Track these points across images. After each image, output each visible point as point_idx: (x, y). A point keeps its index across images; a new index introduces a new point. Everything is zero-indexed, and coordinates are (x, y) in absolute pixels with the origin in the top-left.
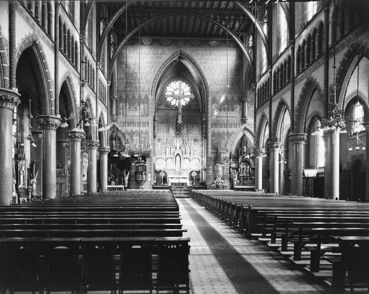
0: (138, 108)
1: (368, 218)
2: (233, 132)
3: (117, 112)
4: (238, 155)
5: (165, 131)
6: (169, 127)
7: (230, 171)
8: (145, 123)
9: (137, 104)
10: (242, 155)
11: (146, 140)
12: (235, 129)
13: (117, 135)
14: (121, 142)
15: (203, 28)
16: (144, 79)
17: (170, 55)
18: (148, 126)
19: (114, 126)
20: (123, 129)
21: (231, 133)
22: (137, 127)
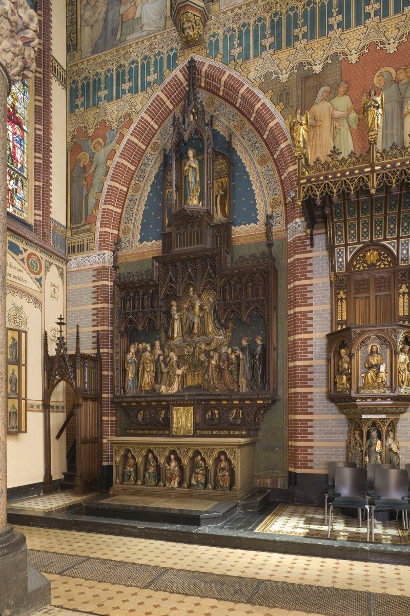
2: (127, 120)
22: (335, 33)
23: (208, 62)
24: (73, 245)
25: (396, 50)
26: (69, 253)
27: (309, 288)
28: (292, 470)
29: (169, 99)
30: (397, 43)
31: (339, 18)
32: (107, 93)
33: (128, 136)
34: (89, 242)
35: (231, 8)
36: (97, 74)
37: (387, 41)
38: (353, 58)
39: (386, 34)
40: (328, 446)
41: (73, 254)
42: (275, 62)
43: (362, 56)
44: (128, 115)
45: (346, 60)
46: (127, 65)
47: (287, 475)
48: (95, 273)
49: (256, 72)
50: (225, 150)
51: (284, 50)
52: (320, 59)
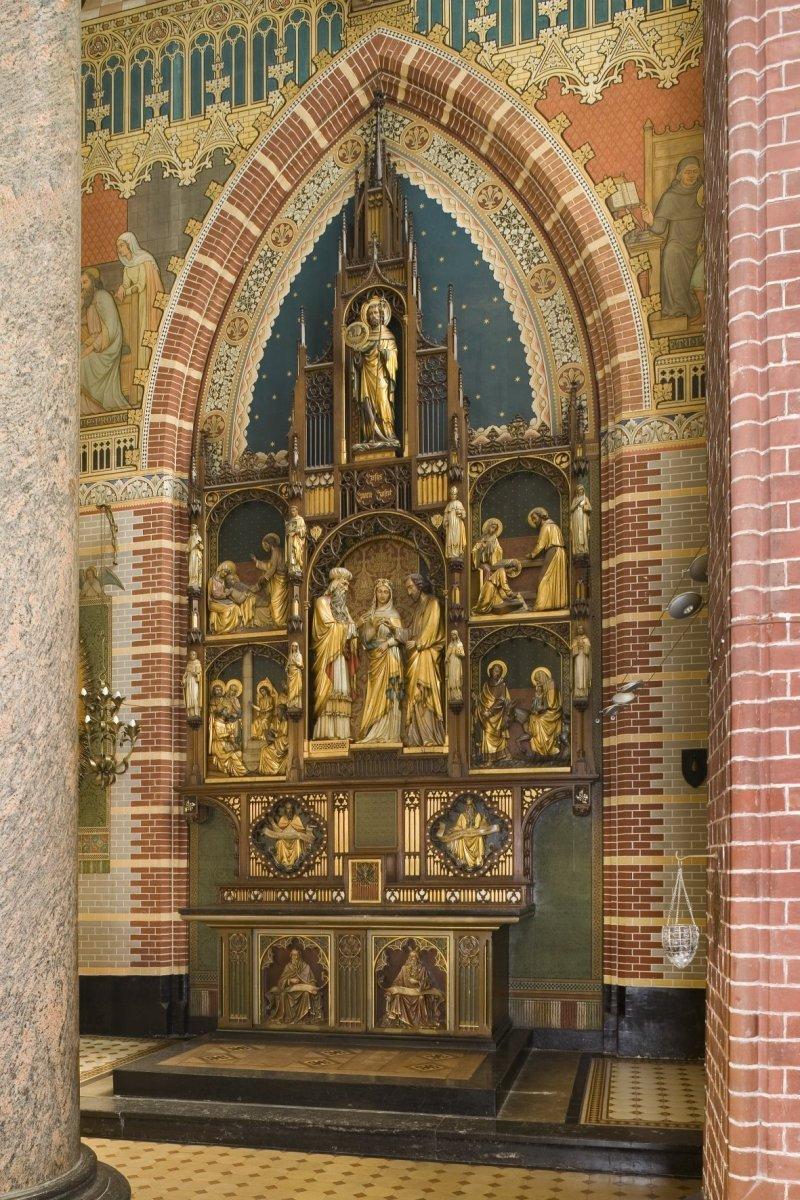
2: (218, 166)
10: (330, 456)
21: (187, 176)
22: (218, 110)
24: (105, 448)
25: (600, 97)
26: (95, 468)
27: (139, 637)
28: (614, 980)
29: (318, 123)
30: (678, 67)
31: (225, 82)
32: (494, 24)
33: (221, 203)
34: (122, 445)
35: (88, 23)
36: (264, 23)
37: (582, 79)
39: (580, 63)
40: (651, 924)
41: (105, 470)
42: (232, 128)
43: (608, 88)
44: (219, 155)
45: (116, 190)
46: (281, 22)
47: (598, 991)
48: (140, 520)
49: (678, 43)
51: (249, 107)
52: (596, 72)
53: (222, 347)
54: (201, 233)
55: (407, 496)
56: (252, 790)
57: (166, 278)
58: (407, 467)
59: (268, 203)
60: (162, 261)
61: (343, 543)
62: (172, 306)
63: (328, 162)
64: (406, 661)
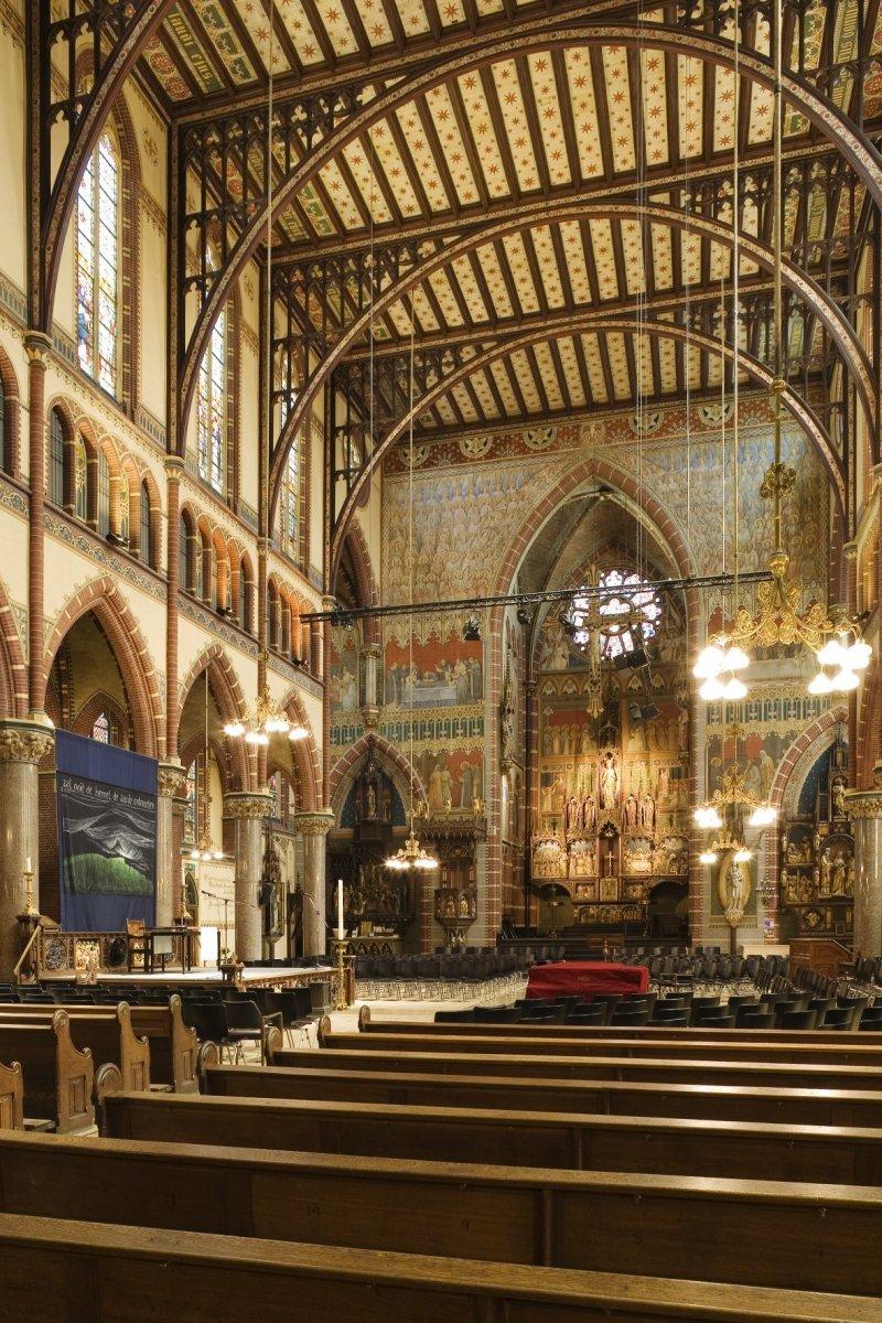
0: (447, 674)
1: (879, 1048)
2: (792, 735)
3: (379, 694)
4: (813, 821)
5: (567, 747)
6: (581, 730)
7: (779, 878)
8: (472, 725)
9: (443, 662)
10: (827, 819)
11: (475, 782)
12: (801, 722)
13: (379, 769)
14: (394, 794)
15: (688, 374)
16: (466, 578)
17: (556, 484)
18: (482, 733)
19: (371, 739)
20: (407, 750)
21: (782, 737)
22: (792, 720)
23: (380, 737)
38: (452, 754)
50: (388, 783)
53: (790, 783)
54: (787, 753)
55: (848, 831)
56: (800, 906)
57: (776, 765)
58: (849, 824)
59: (804, 745)
60: (774, 759)
61: (830, 840)
62: (777, 773)
63: (823, 735)
64: (847, 873)
